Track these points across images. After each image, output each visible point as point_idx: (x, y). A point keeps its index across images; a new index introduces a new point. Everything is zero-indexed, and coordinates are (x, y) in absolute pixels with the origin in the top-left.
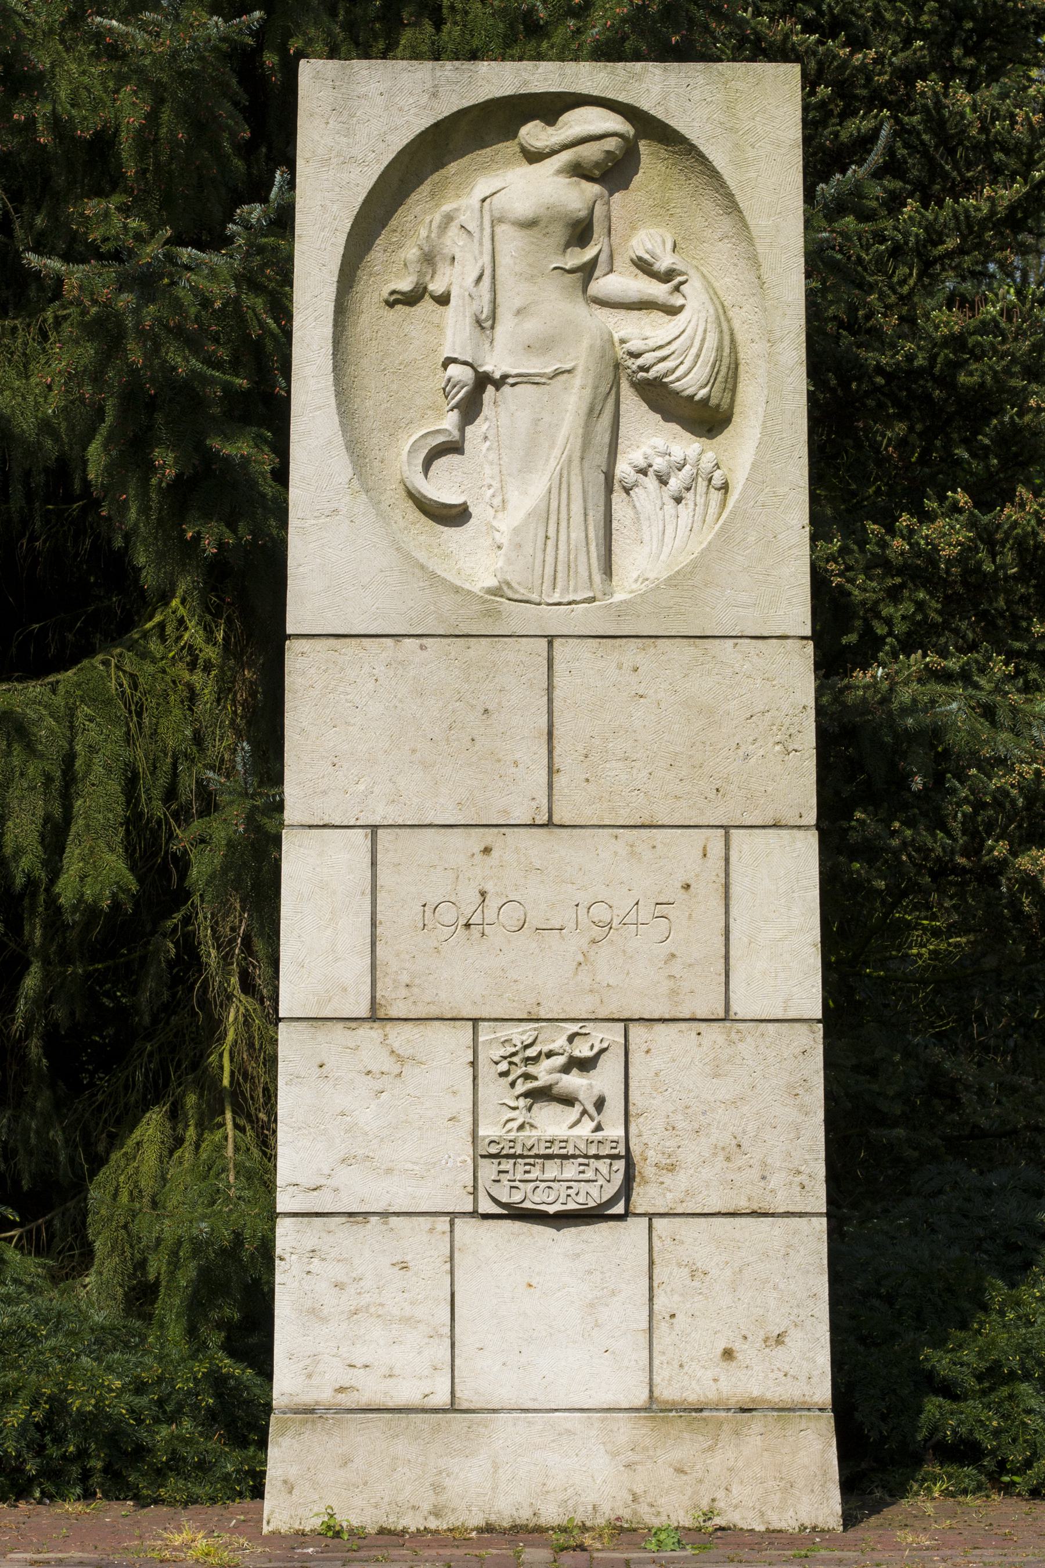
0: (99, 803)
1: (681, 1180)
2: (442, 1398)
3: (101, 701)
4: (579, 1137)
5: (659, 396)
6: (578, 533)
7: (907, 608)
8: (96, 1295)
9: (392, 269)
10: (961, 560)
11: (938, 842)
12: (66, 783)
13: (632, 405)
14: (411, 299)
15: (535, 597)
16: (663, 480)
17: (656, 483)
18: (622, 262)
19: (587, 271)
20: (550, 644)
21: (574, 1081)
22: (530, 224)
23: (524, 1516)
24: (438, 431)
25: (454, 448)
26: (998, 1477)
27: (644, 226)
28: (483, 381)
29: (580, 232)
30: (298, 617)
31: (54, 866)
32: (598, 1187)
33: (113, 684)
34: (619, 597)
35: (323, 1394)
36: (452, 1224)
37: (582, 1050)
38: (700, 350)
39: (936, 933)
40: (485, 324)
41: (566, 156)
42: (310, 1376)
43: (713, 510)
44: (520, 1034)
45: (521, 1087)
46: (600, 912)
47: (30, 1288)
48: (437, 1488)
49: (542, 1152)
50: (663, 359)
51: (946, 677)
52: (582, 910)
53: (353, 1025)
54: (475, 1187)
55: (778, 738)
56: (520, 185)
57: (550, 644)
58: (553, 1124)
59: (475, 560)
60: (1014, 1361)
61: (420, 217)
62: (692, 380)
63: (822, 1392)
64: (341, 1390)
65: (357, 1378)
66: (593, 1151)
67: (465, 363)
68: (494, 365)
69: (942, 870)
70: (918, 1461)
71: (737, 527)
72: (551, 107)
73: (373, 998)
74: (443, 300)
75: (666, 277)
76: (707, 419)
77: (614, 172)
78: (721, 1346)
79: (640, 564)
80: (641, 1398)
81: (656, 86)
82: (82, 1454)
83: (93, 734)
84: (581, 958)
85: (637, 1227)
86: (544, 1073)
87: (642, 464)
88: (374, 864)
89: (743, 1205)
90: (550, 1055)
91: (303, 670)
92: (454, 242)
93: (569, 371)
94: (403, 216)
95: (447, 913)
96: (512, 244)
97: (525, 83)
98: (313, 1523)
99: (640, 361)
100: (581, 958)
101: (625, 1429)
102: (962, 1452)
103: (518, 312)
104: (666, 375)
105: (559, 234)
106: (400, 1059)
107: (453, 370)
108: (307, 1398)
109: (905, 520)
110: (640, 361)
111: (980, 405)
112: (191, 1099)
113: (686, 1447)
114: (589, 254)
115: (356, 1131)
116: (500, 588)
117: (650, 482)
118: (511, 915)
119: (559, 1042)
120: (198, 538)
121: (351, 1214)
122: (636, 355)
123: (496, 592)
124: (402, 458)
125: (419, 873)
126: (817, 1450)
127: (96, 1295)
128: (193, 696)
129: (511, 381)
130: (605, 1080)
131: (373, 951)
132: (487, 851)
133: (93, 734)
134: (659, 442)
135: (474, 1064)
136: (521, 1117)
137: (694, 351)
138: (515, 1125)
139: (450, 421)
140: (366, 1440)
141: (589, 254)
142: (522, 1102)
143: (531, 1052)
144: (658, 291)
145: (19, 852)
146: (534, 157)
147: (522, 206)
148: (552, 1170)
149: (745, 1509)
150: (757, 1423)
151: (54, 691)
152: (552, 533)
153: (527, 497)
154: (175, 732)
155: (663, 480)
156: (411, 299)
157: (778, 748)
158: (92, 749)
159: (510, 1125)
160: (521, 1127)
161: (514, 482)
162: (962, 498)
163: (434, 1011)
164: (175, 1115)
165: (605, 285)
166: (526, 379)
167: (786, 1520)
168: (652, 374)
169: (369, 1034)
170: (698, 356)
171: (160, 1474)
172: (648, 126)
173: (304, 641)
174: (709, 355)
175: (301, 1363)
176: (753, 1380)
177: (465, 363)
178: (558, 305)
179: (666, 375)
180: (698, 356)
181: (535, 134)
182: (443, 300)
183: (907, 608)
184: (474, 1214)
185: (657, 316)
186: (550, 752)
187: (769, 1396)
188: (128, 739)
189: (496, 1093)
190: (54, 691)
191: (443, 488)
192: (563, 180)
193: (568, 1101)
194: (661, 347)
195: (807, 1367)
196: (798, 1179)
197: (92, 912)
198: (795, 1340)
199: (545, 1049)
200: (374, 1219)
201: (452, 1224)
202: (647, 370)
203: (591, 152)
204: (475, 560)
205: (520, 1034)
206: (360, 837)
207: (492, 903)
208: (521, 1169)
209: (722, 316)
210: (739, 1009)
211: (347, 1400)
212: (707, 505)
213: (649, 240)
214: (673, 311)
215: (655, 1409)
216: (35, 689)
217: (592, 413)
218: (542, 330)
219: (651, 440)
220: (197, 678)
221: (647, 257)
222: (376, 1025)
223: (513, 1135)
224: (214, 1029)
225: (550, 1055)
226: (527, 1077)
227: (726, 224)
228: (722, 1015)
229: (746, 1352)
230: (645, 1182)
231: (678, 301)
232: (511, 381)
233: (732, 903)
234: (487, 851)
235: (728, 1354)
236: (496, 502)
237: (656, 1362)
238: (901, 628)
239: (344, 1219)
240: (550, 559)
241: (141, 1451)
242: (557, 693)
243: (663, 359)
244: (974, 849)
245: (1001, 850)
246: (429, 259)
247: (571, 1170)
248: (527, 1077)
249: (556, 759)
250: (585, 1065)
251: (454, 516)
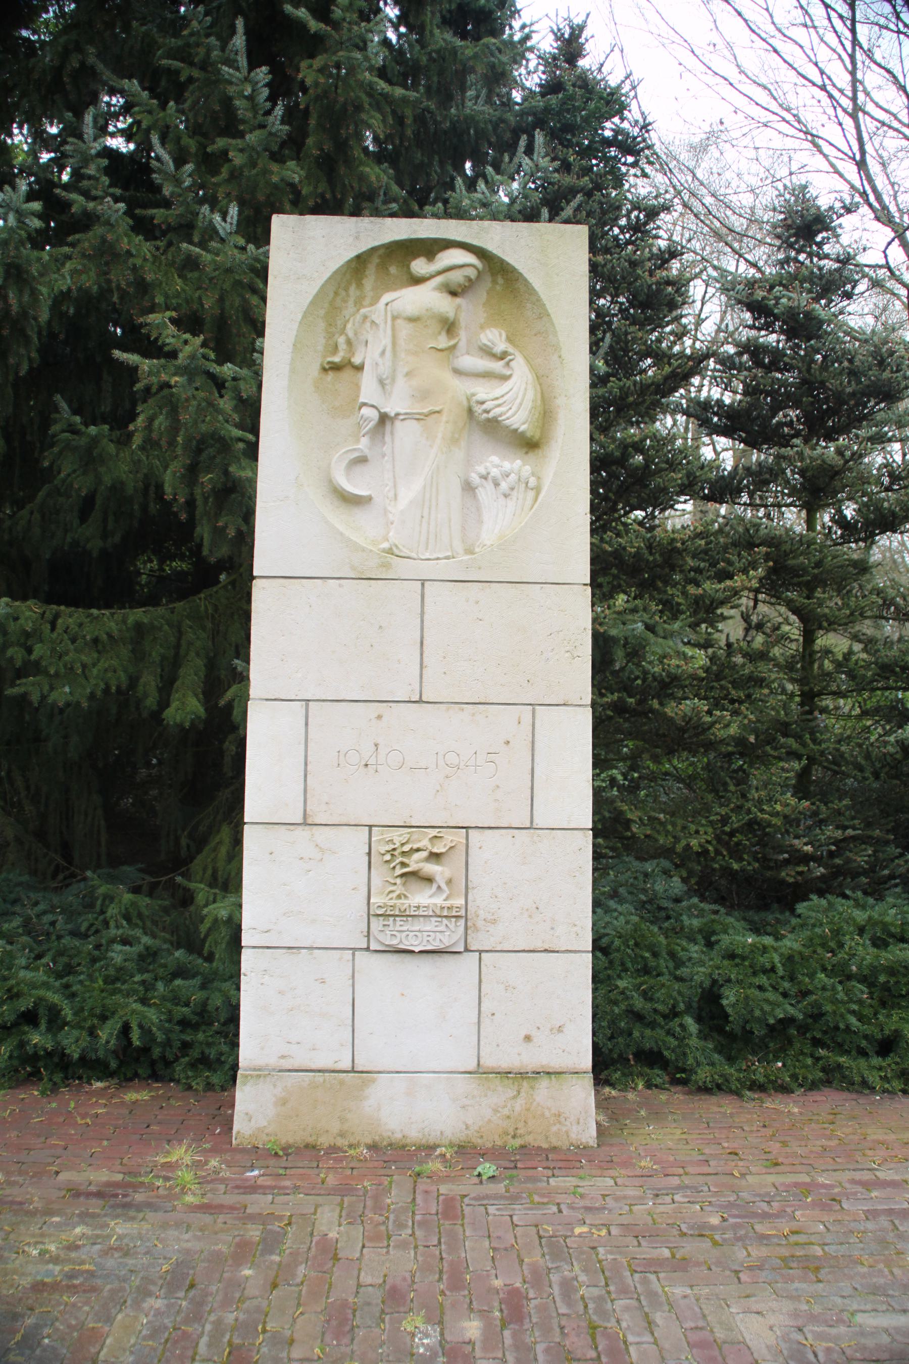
4: (435, 905)
15: (414, 555)
16: (497, 484)
17: (492, 486)
20: (423, 585)
21: (431, 868)
24: (355, 450)
28: (384, 419)
31: (164, 704)
32: (448, 935)
33: (203, 608)
36: (354, 955)
38: (523, 400)
41: (439, 279)
42: (262, 1048)
43: (529, 502)
44: (398, 836)
45: (399, 871)
46: (452, 758)
48: (342, 1120)
49: (413, 913)
50: (499, 406)
52: (440, 757)
53: (292, 827)
54: (368, 932)
55: (567, 648)
57: (423, 585)
58: (422, 897)
62: (519, 418)
64: (283, 1057)
66: (445, 914)
67: (373, 406)
68: (390, 409)
72: (430, 248)
73: (305, 811)
74: (360, 368)
75: (502, 356)
76: (529, 444)
78: (524, 1033)
83: (190, 636)
84: (439, 788)
86: (415, 863)
87: (484, 472)
88: (307, 724)
89: (539, 946)
90: (418, 850)
93: (438, 412)
97: (415, 232)
99: (484, 406)
100: (439, 788)
101: (463, 1084)
103: (407, 374)
104: (500, 415)
106: (322, 850)
107: (364, 410)
108: (261, 1062)
110: (484, 406)
115: (291, 887)
116: (391, 549)
117: (489, 485)
119: (424, 843)
120: (225, 527)
121: (289, 948)
122: (483, 403)
123: (390, 551)
129: (401, 417)
131: (305, 780)
132: (379, 717)
134: (495, 459)
135: (369, 854)
136: (399, 890)
137: (518, 401)
138: (394, 895)
142: (398, 881)
143: (406, 848)
144: (497, 366)
145: (146, 695)
146: (417, 281)
151: (173, 612)
152: (426, 514)
153: (409, 492)
155: (497, 484)
157: (567, 655)
158: (190, 644)
159: (391, 896)
160: (399, 897)
163: (344, 820)
168: (491, 415)
169: (302, 833)
170: (521, 404)
173: (264, 580)
177: (373, 406)
179: (500, 415)
180: (521, 404)
181: (419, 266)
184: (368, 949)
185: (495, 382)
186: (422, 655)
187: (552, 1064)
190: (173, 612)
193: (429, 880)
194: (497, 399)
196: (575, 929)
197: (180, 726)
199: (415, 846)
200: (303, 951)
201: (354, 955)
202: (488, 412)
203: (457, 277)
205: (398, 836)
207: (382, 751)
208: (399, 923)
210: (539, 822)
211: (287, 1064)
212: (525, 499)
214: (505, 378)
215: (480, 1072)
219: (499, 462)
221: (489, 344)
222: (307, 828)
223: (391, 903)
225: (418, 850)
226: (403, 865)
228: (528, 825)
230: (477, 930)
231: (507, 372)
232: (401, 417)
233: (536, 753)
234: (379, 717)
235: (528, 1038)
236: (391, 494)
237: (482, 1043)
239: (284, 951)
242: (426, 617)
243: (499, 406)
248: (403, 865)
249: (425, 659)
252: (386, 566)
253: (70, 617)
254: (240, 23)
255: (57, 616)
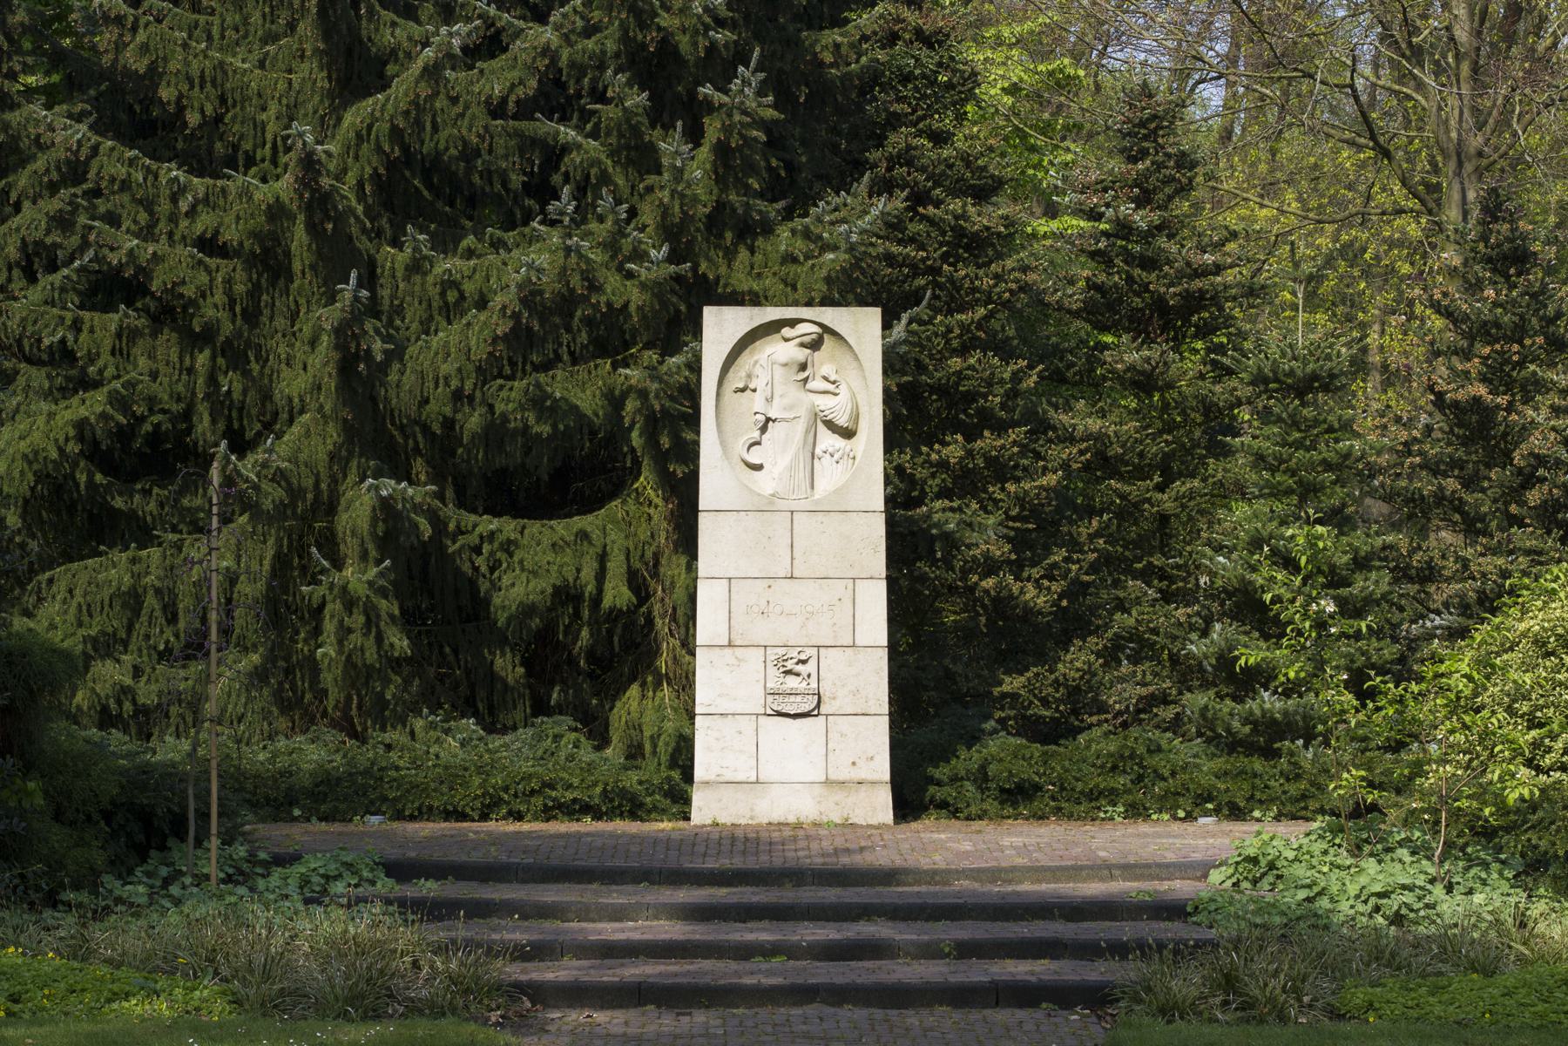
0: (616, 566)
1: (837, 703)
2: (753, 779)
3: (614, 521)
5: (831, 425)
6: (802, 475)
7: (937, 481)
8: (614, 753)
9: (736, 379)
10: (959, 463)
11: (951, 576)
12: (603, 558)
13: (821, 428)
14: (743, 390)
18: (818, 377)
19: (805, 380)
21: (800, 668)
22: (786, 365)
23: (782, 820)
25: (758, 443)
26: (954, 813)
27: (826, 363)
28: (768, 420)
29: (803, 367)
30: (703, 504)
34: (817, 497)
35: (712, 777)
37: (803, 657)
39: (955, 613)
40: (769, 400)
46: (809, 609)
47: (970, 525)
51: (952, 510)
56: (780, 350)
58: (792, 682)
59: (764, 483)
60: (963, 773)
61: (746, 361)
62: (842, 421)
63: (887, 777)
65: (724, 772)
69: (952, 589)
70: (926, 809)
71: (859, 473)
72: (793, 323)
76: (848, 433)
77: (815, 345)
79: (824, 485)
80: (823, 779)
81: (829, 315)
82: (620, 805)
83: (613, 536)
85: (822, 719)
86: (790, 665)
91: (705, 523)
92: (758, 370)
94: (740, 360)
95: (755, 609)
96: (779, 372)
98: (709, 822)
101: (817, 789)
102: (943, 805)
105: (796, 368)
108: (706, 778)
109: (936, 446)
111: (971, 397)
112: (650, 679)
113: (838, 796)
114: (805, 374)
115: (725, 683)
118: (778, 610)
119: (795, 654)
124: (739, 448)
125: (747, 594)
126: (885, 798)
127: (614, 753)
128: (650, 518)
130: (810, 667)
133: (613, 536)
139: (756, 434)
140: (727, 793)
141: (805, 374)
144: (831, 387)
146: (786, 340)
147: (783, 360)
148: (792, 698)
149: (859, 818)
150: (863, 787)
153: (784, 461)
154: (644, 535)
156: (743, 390)
158: (613, 542)
161: (780, 452)
162: (959, 437)
164: (643, 685)
165: (811, 385)
166: (784, 420)
167: (874, 822)
169: (728, 651)
171: (649, 812)
172: (827, 329)
174: (848, 411)
175: (704, 765)
176: (863, 773)
178: (795, 393)
181: (786, 332)
182: (754, 390)
183: (937, 481)
188: (627, 537)
189: (773, 672)
191: (754, 458)
192: (798, 349)
193: (798, 675)
195: (881, 767)
198: (877, 759)
203: (807, 339)
204: (764, 483)
206: (725, 582)
209: (853, 396)
210: (858, 643)
213: (827, 369)
215: (828, 782)
216: (590, 518)
217: (807, 432)
218: (790, 402)
219: (828, 440)
220: (652, 511)
224: (657, 652)
227: (855, 364)
229: (860, 763)
238: (936, 489)
240: (761, 933)
241: (642, 805)
244: (964, 578)
245: (975, 578)
246: (749, 376)
247: (799, 698)
250: (804, 662)
251: (758, 468)
252: (771, 503)
253: (534, 527)
254: (679, 124)
255: (524, 527)
